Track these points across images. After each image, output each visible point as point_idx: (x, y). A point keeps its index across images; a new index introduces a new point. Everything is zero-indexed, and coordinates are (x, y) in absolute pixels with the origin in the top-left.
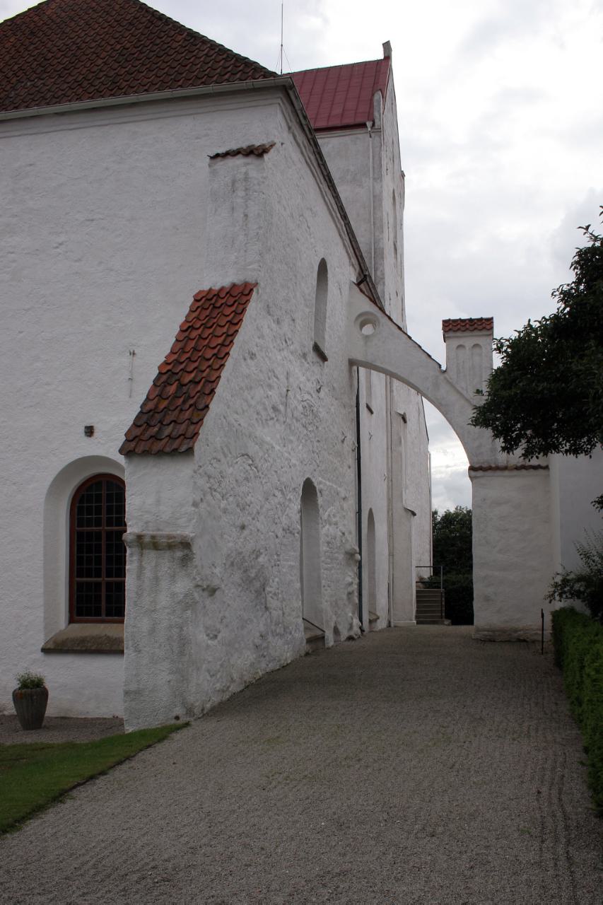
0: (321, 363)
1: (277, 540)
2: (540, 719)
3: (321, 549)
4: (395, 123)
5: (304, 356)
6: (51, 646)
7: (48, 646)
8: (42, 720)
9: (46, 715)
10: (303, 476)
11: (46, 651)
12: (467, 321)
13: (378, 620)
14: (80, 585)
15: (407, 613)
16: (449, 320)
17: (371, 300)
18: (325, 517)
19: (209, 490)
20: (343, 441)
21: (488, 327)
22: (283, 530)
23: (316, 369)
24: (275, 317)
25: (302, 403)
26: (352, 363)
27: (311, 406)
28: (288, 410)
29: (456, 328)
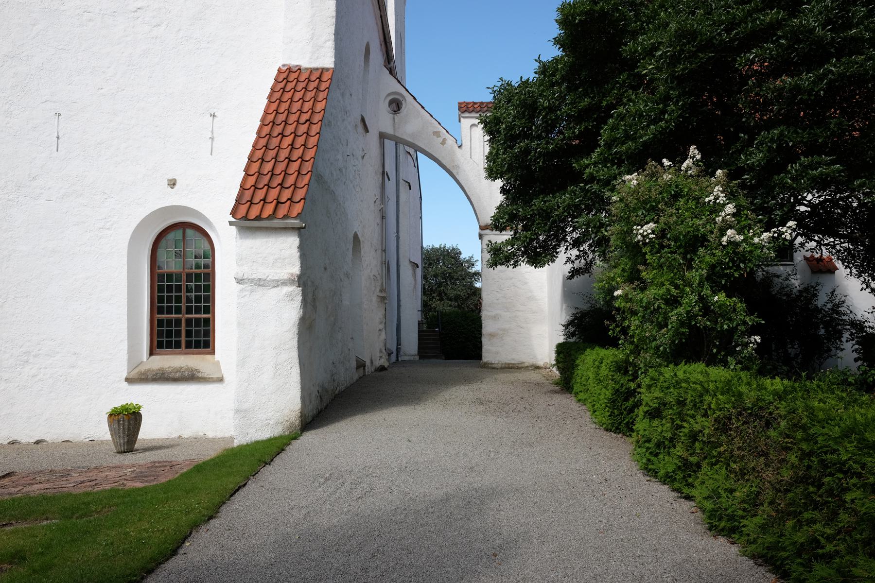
0: (364, 134)
2: (851, 272)
6: (134, 374)
7: (131, 377)
8: (135, 442)
9: (140, 436)
11: (127, 380)
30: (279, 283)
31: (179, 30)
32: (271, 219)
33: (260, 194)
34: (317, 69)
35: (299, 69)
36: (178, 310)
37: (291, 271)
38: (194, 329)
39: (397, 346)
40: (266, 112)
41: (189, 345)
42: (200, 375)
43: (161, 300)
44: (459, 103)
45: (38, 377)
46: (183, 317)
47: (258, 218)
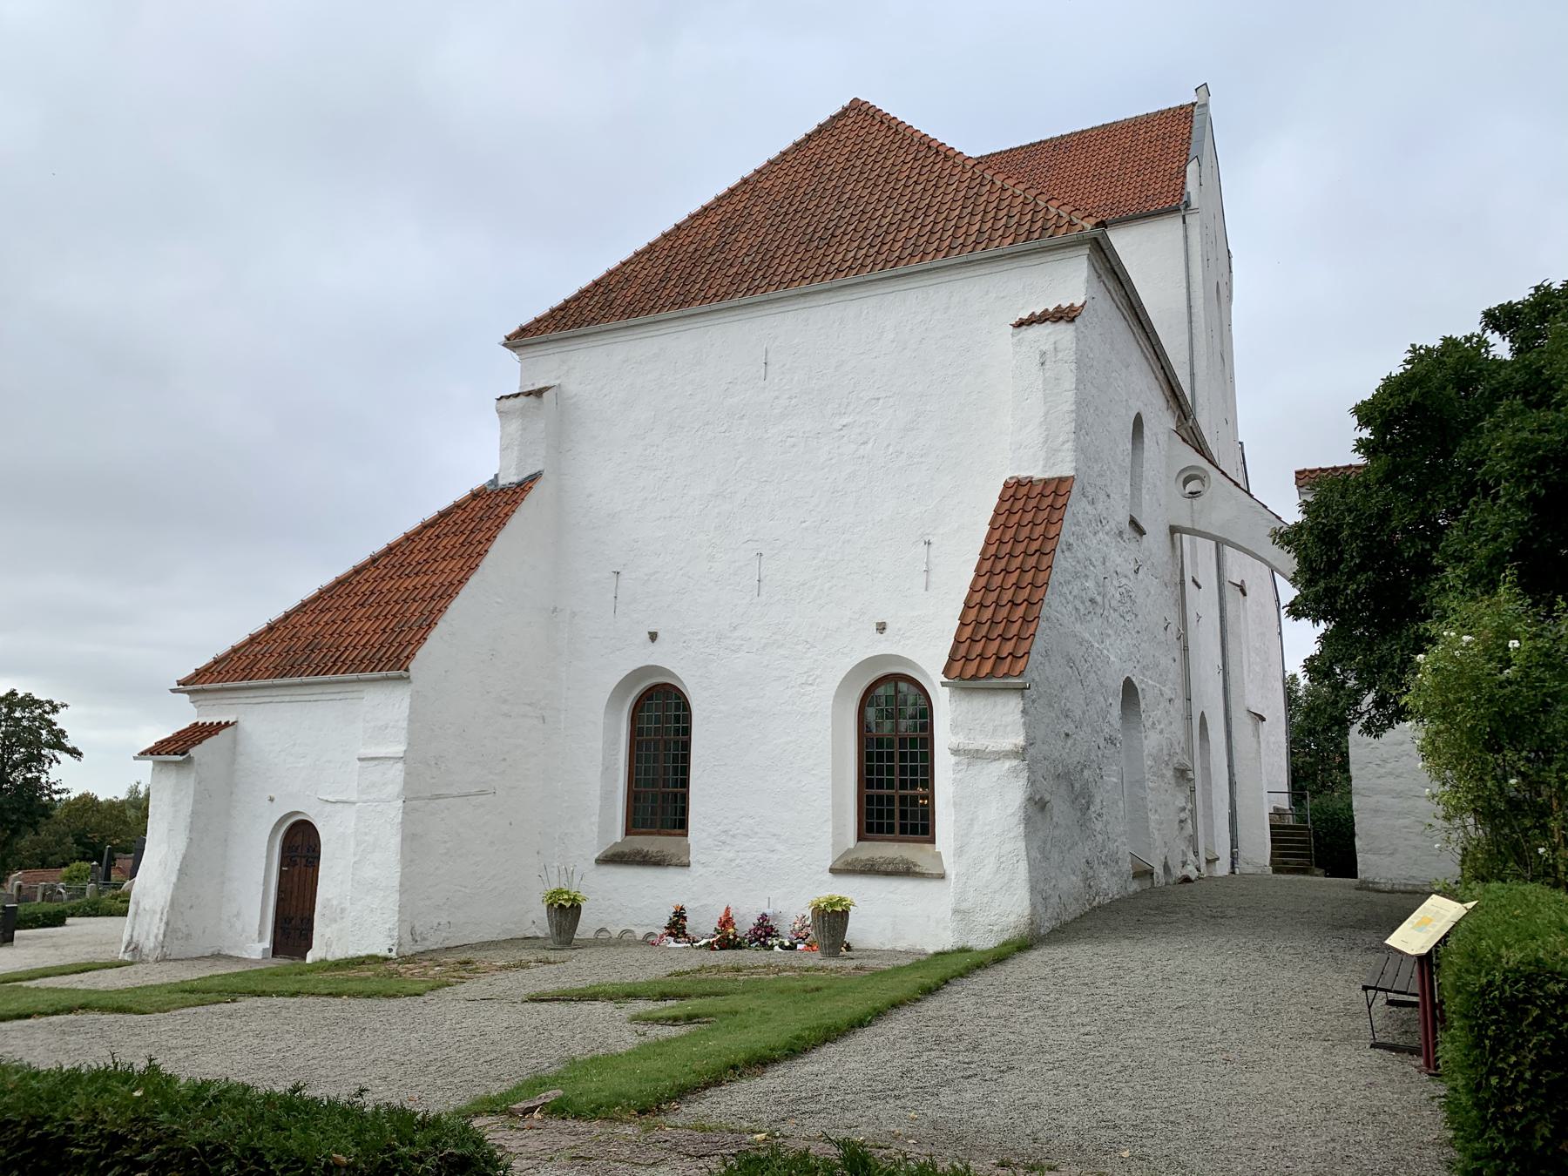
0: (1138, 537)
4: (1208, 126)
7: (837, 867)
11: (832, 871)
15: (1258, 848)
17: (1197, 450)
18: (1148, 724)
20: (1166, 629)
23: (1133, 546)
24: (1090, 498)
26: (1173, 530)
27: (1128, 591)
28: (1106, 600)
30: (1007, 755)
31: (889, 445)
32: (989, 678)
33: (978, 648)
34: (1053, 479)
35: (1031, 481)
36: (890, 785)
37: (1014, 741)
38: (885, 808)
39: (1232, 849)
40: (987, 543)
41: (903, 830)
42: (917, 870)
43: (870, 771)
44: (1296, 473)
45: (737, 862)
46: (897, 793)
47: (974, 677)
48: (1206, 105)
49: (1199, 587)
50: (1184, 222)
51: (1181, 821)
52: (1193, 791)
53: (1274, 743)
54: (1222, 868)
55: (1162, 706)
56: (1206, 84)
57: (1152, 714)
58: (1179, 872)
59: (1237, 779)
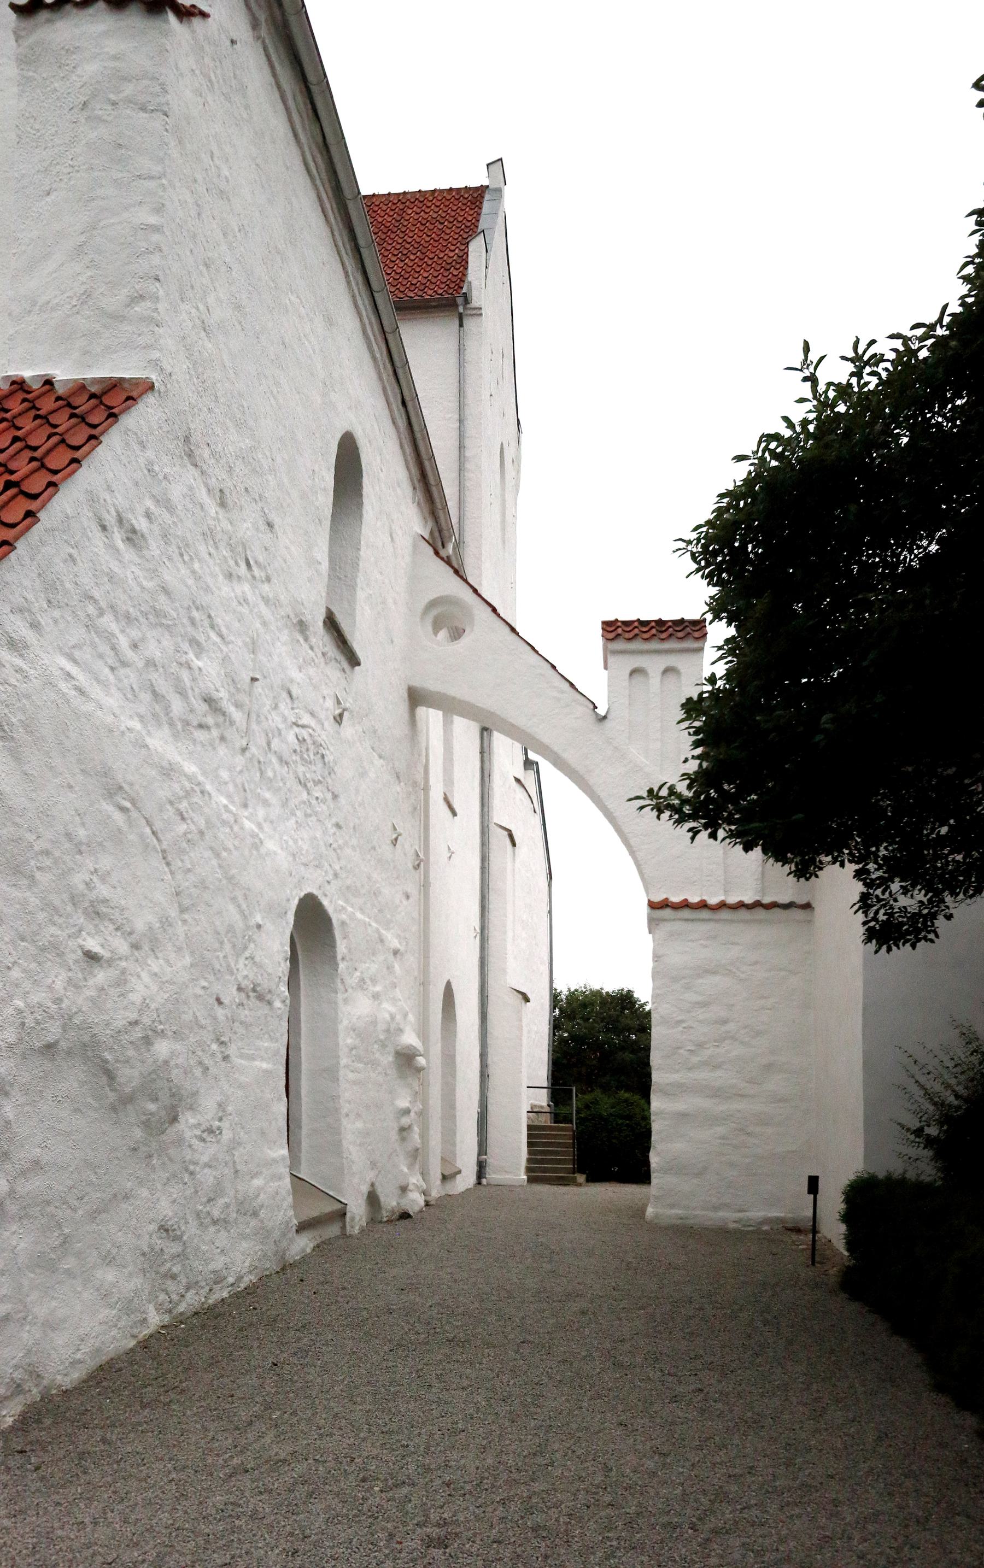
1: (220, 1012)
3: (341, 1043)
5: (302, 626)
10: (299, 884)
12: (653, 624)
13: (458, 1176)
14: (562, 1041)
16: (617, 620)
18: (352, 981)
19: (277, 979)
21: (697, 634)
22: (240, 989)
25: (296, 729)
29: (631, 635)
39: (479, 1155)
48: (499, 191)
49: (454, 814)
50: (461, 325)
51: (402, 1130)
52: (424, 1085)
53: (536, 1033)
54: (466, 1180)
55: (381, 958)
56: (501, 160)
57: (364, 966)
58: (390, 1202)
59: (492, 1070)
